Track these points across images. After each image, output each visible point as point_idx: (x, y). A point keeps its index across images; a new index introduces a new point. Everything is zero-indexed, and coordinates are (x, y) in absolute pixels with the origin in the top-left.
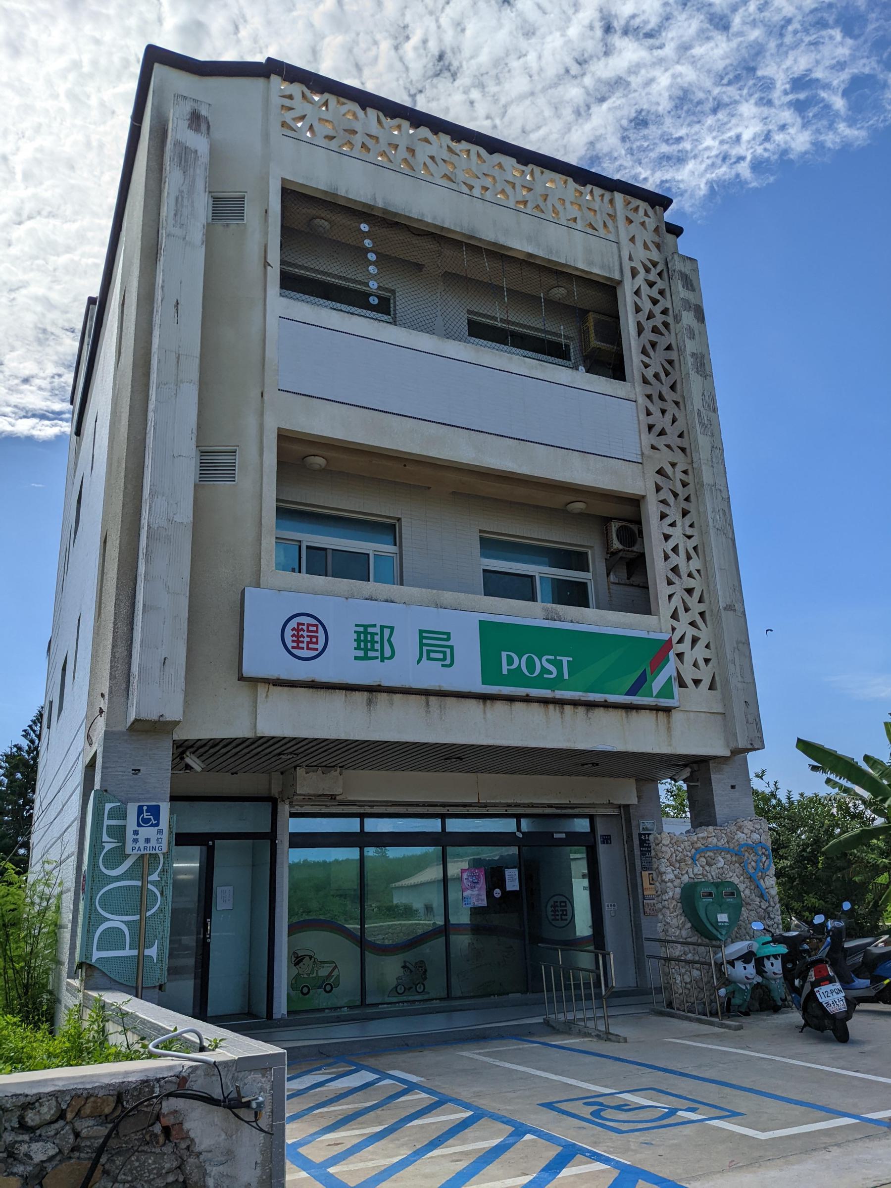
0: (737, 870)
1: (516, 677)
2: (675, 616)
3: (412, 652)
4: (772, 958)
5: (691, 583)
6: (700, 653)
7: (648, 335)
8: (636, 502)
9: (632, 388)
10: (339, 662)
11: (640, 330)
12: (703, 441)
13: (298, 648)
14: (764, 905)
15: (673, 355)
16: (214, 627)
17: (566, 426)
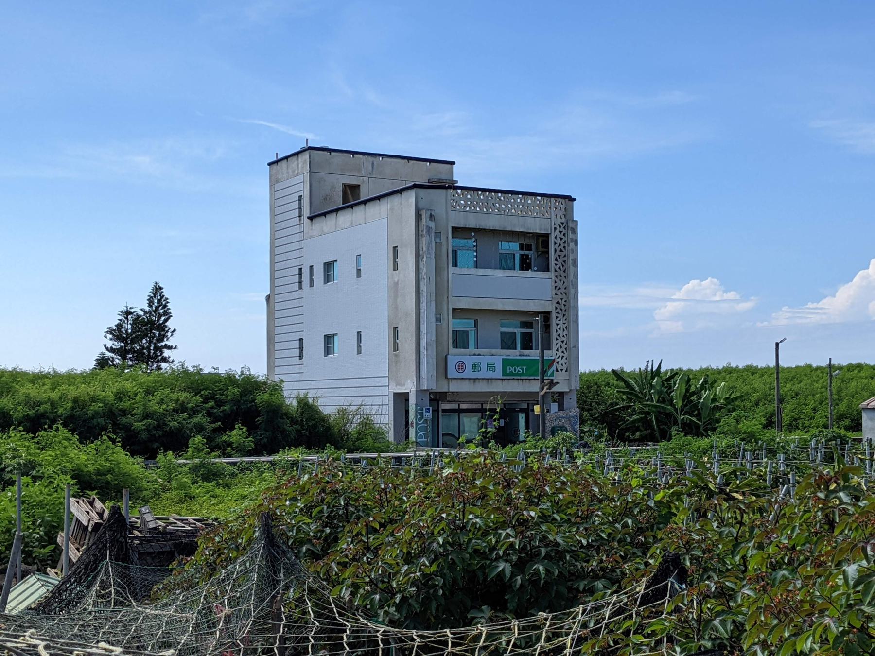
1: (511, 374)
2: (557, 350)
3: (486, 371)
5: (563, 339)
6: (564, 360)
7: (558, 253)
8: (549, 313)
9: (551, 274)
10: (469, 373)
11: (555, 251)
12: (572, 291)
15: (566, 259)
16: (442, 366)
17: (528, 290)
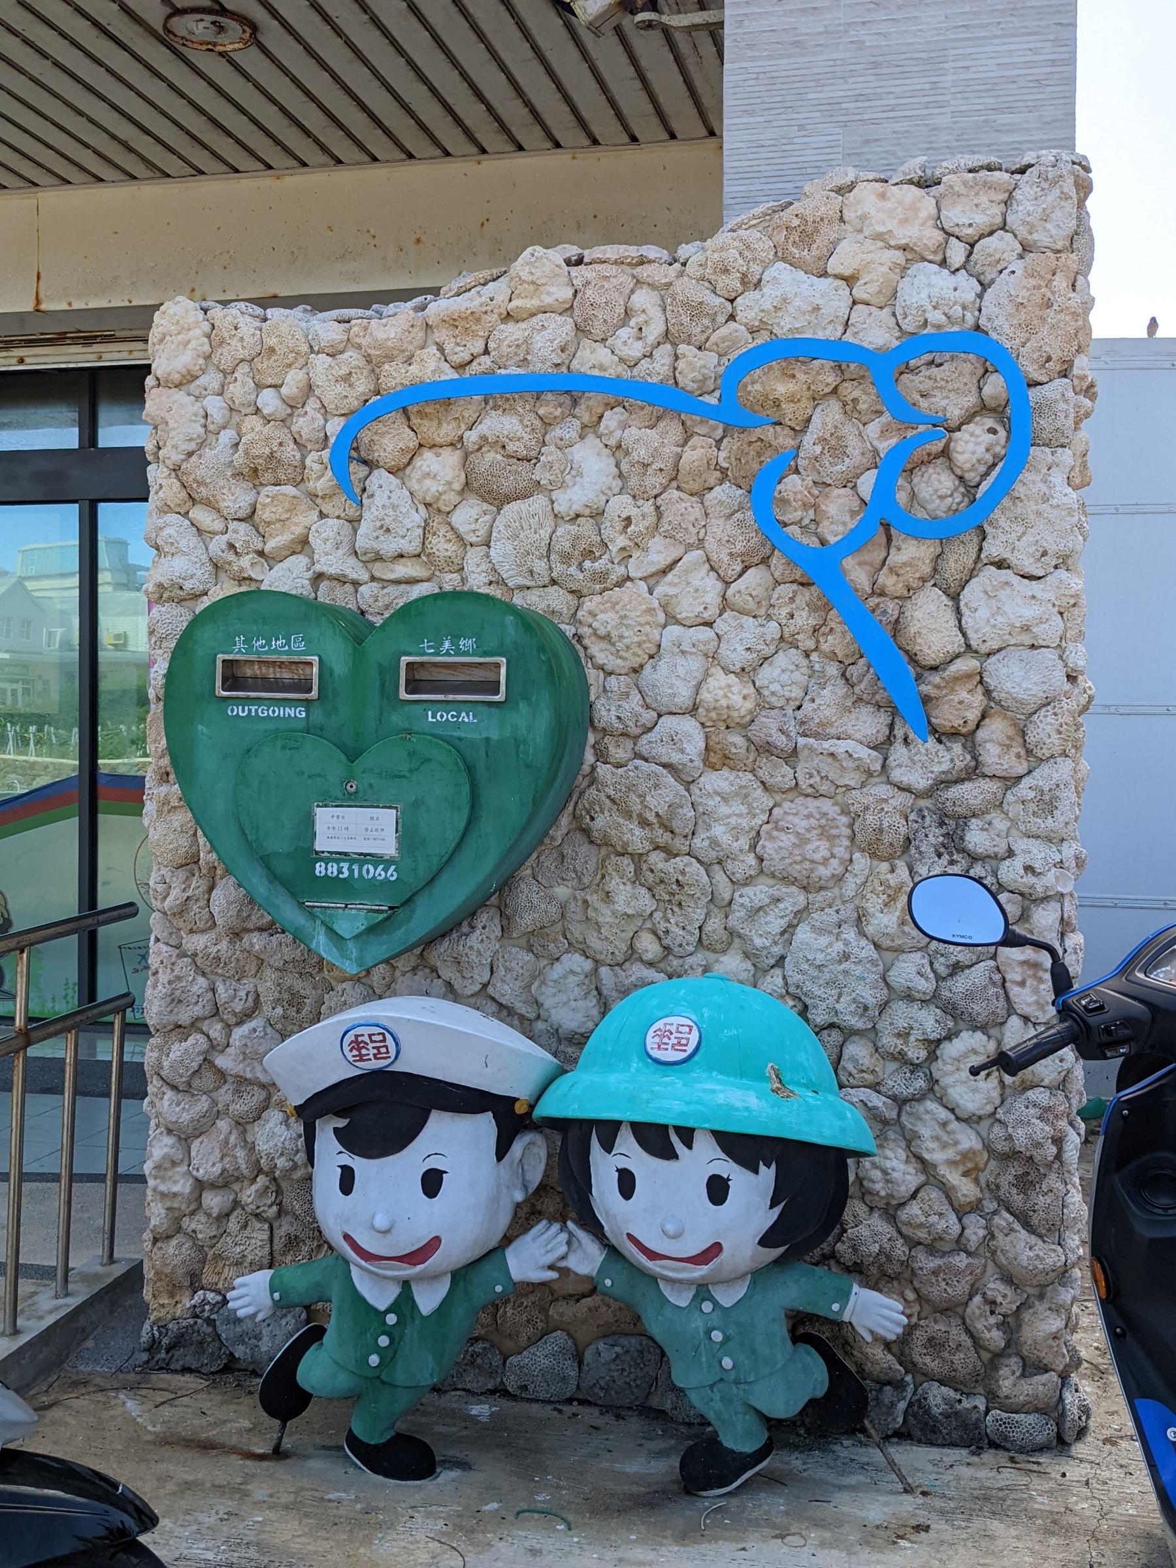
0: (719, 529)
4: (626, 1142)
13: (361, 1060)
14: (921, 763)
